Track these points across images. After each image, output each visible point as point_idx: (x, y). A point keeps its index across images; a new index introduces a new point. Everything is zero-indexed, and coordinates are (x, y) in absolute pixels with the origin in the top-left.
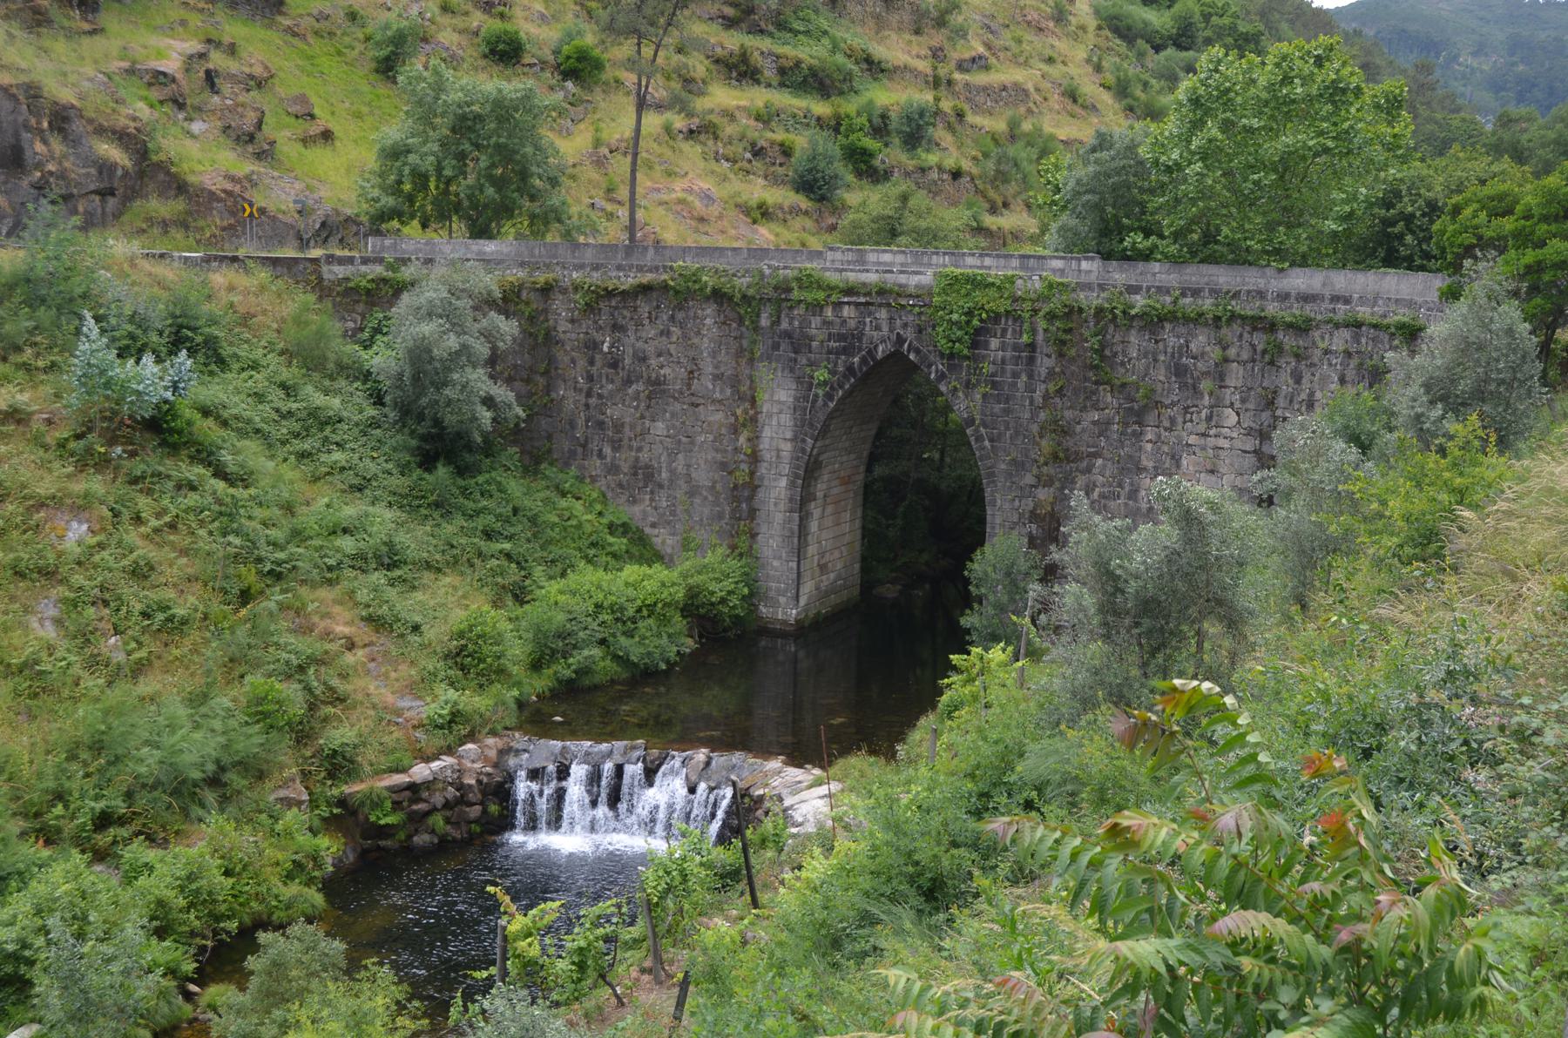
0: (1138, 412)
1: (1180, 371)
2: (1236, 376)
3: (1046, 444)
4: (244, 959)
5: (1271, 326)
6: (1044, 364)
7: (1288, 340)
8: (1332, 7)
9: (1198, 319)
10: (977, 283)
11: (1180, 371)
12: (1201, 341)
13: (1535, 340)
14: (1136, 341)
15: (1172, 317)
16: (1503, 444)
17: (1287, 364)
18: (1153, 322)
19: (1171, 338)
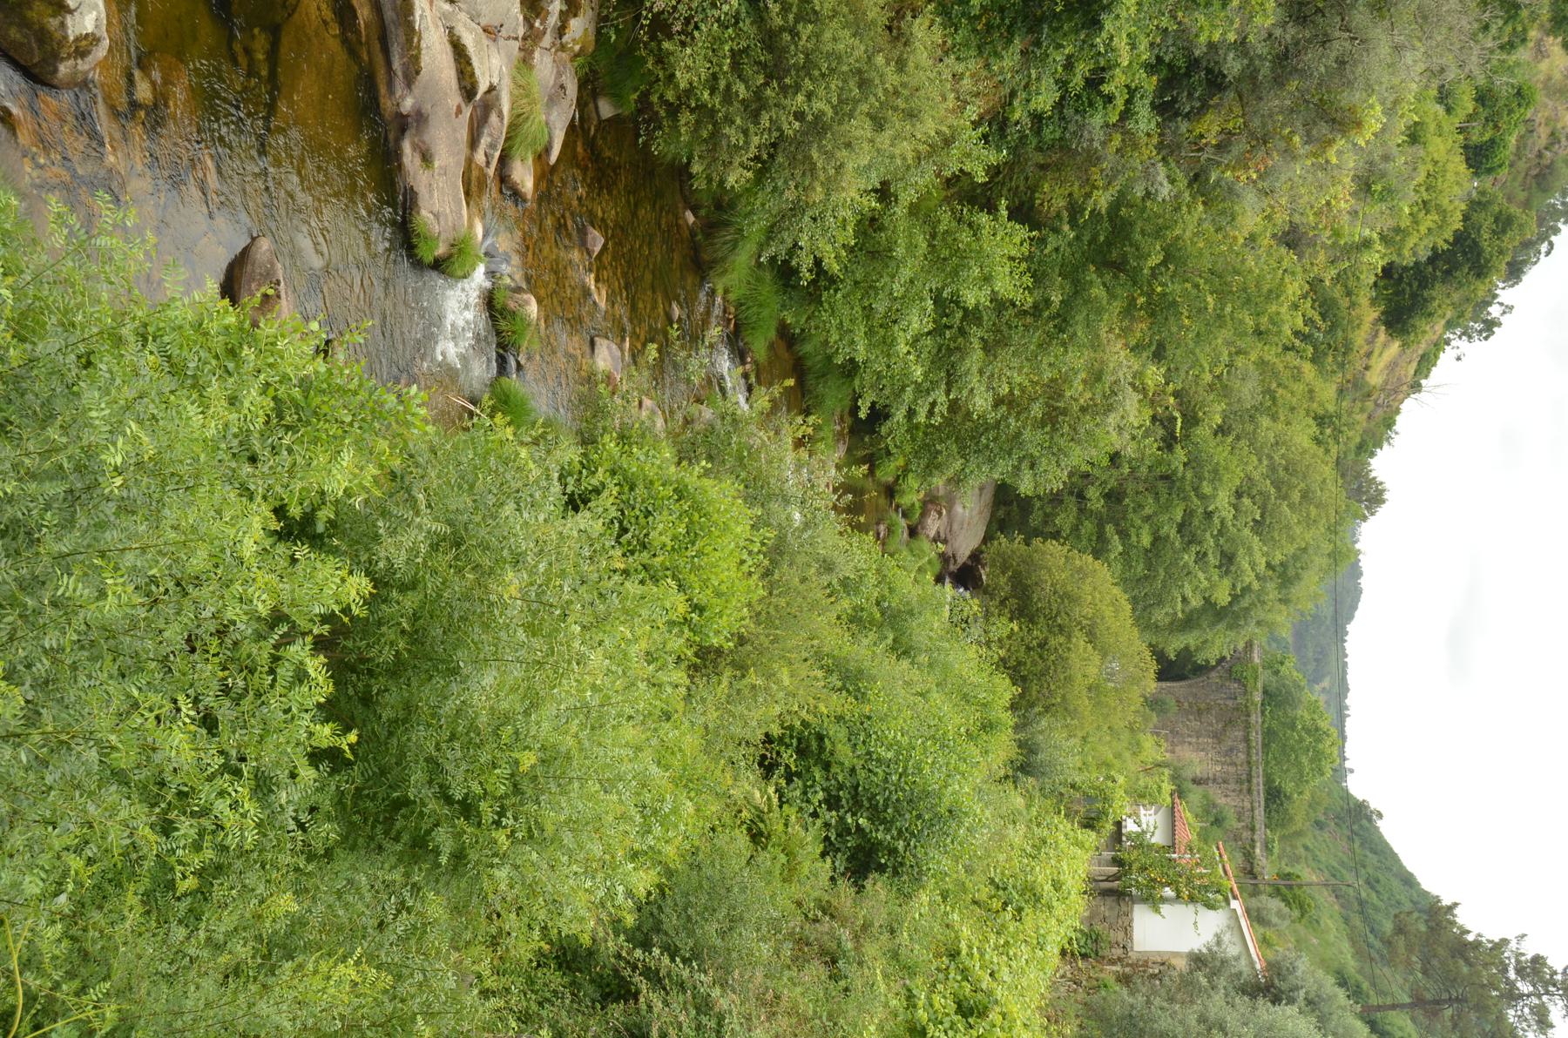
0: (1218, 737)
1: (1231, 750)
2: (1232, 769)
3: (1203, 706)
4: (56, 70)
5: (1249, 781)
6: (1230, 703)
7: (1245, 786)
8: (1349, 646)
9: (1249, 754)
10: (1256, 679)
11: (1231, 750)
12: (1242, 756)
13: (1434, 293)
14: (1239, 734)
15: (1249, 747)
16: (1479, 276)
17: (1237, 787)
18: (1247, 740)
19: (1242, 746)
